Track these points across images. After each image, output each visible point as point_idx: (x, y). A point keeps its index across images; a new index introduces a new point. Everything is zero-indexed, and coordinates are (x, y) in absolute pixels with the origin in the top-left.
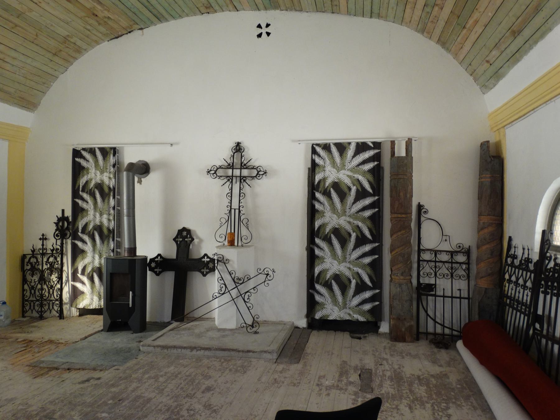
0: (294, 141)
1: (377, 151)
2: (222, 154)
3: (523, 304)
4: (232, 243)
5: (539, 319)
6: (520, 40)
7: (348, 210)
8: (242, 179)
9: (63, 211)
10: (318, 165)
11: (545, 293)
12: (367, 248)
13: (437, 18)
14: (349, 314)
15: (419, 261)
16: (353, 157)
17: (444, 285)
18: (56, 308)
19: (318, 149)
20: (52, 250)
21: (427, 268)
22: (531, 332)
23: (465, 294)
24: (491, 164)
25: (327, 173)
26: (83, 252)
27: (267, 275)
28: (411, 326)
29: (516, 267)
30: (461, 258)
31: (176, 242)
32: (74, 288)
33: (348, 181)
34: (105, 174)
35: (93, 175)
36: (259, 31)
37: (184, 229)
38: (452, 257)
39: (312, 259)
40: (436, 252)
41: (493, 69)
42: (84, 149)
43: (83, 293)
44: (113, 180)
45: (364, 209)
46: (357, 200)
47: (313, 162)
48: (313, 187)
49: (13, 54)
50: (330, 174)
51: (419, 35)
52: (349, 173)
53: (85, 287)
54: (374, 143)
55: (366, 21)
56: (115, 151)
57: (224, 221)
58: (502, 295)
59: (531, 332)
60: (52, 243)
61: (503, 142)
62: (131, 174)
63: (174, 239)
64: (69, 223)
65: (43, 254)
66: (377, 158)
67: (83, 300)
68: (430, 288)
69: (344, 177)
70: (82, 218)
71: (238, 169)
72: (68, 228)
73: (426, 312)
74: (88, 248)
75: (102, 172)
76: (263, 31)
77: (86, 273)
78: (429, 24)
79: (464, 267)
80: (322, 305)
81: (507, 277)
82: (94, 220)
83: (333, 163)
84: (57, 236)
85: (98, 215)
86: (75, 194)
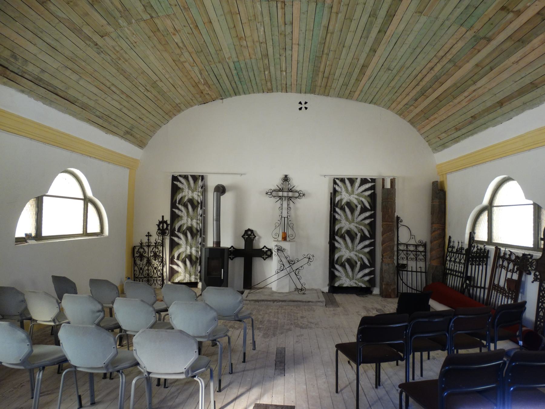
0: (322, 176)
1: (373, 184)
2: (275, 182)
3: (459, 272)
4: (284, 239)
5: (469, 278)
6: (459, 133)
7: (355, 219)
8: (289, 198)
9: (163, 217)
10: (337, 191)
11: (472, 265)
12: (367, 242)
13: (412, 111)
14: (356, 283)
15: (398, 250)
16: (359, 187)
17: (412, 265)
18: (159, 283)
19: (338, 181)
20: (155, 243)
21: (402, 255)
22: (465, 286)
23: (423, 270)
24: (438, 194)
25: (343, 196)
26: (178, 244)
27: (309, 258)
28: (394, 289)
29: (454, 253)
30: (421, 249)
31: (244, 238)
32: (172, 269)
33: (355, 202)
34: (195, 193)
35: (187, 193)
36: (300, 106)
37: (249, 230)
38: (407, 247)
39: (333, 249)
40: (407, 245)
41: (442, 142)
42: (180, 176)
43: (177, 272)
44: (201, 197)
45: (366, 218)
46: (361, 213)
47: (334, 189)
48: (334, 205)
49: (148, 115)
50: (344, 197)
51: (398, 116)
52: (357, 197)
53: (180, 268)
54: (371, 179)
55: (367, 105)
56: (203, 178)
57: (277, 225)
58: (445, 269)
59: (465, 286)
60: (155, 238)
61: (445, 182)
62: (219, 193)
63: (242, 236)
64: (167, 225)
65: (149, 246)
66: (373, 188)
67: (178, 277)
68: (404, 266)
69: (353, 199)
70: (178, 222)
71: (286, 192)
72: (167, 229)
73: (402, 280)
74: (182, 242)
75: (193, 192)
76: (303, 106)
77: (180, 259)
78: (406, 112)
79: (423, 254)
80: (339, 278)
81: (448, 258)
82: (187, 223)
83: (347, 191)
84: (159, 233)
85: (189, 220)
86: (173, 205)
